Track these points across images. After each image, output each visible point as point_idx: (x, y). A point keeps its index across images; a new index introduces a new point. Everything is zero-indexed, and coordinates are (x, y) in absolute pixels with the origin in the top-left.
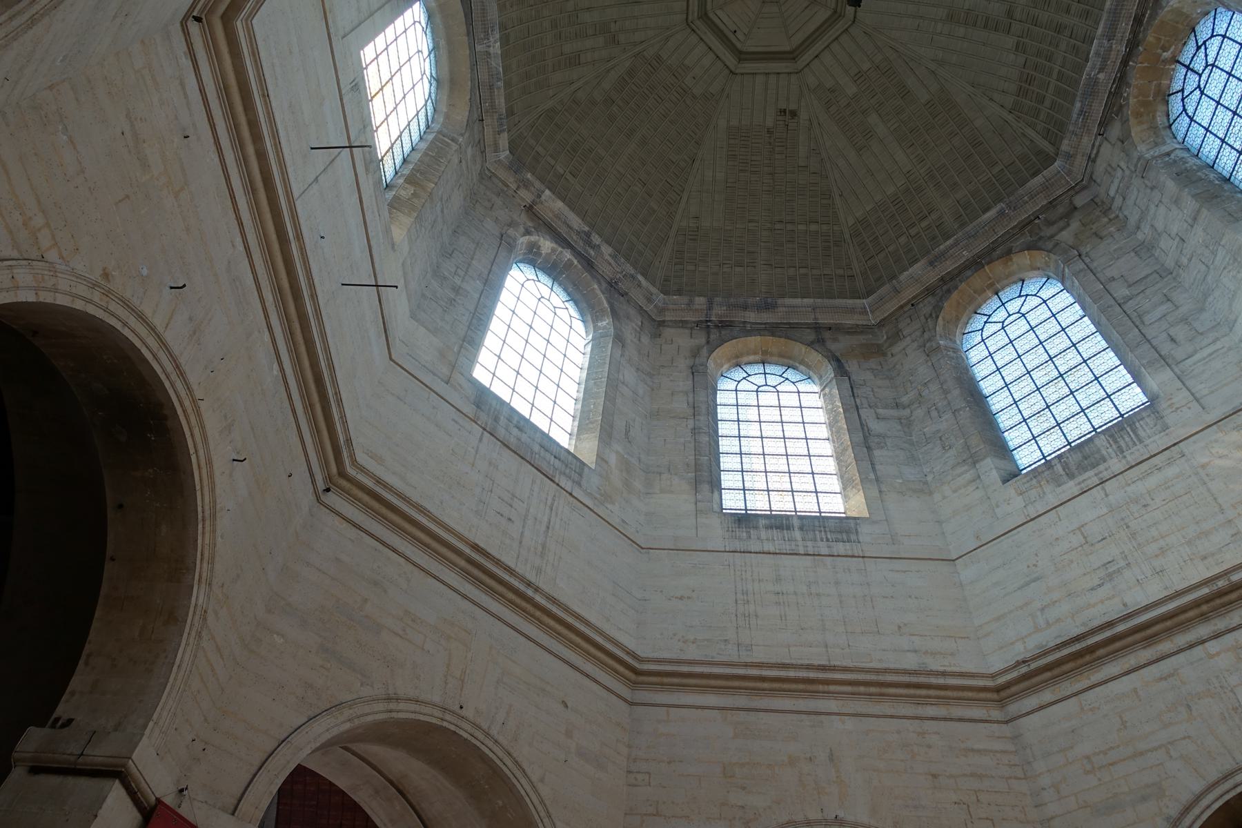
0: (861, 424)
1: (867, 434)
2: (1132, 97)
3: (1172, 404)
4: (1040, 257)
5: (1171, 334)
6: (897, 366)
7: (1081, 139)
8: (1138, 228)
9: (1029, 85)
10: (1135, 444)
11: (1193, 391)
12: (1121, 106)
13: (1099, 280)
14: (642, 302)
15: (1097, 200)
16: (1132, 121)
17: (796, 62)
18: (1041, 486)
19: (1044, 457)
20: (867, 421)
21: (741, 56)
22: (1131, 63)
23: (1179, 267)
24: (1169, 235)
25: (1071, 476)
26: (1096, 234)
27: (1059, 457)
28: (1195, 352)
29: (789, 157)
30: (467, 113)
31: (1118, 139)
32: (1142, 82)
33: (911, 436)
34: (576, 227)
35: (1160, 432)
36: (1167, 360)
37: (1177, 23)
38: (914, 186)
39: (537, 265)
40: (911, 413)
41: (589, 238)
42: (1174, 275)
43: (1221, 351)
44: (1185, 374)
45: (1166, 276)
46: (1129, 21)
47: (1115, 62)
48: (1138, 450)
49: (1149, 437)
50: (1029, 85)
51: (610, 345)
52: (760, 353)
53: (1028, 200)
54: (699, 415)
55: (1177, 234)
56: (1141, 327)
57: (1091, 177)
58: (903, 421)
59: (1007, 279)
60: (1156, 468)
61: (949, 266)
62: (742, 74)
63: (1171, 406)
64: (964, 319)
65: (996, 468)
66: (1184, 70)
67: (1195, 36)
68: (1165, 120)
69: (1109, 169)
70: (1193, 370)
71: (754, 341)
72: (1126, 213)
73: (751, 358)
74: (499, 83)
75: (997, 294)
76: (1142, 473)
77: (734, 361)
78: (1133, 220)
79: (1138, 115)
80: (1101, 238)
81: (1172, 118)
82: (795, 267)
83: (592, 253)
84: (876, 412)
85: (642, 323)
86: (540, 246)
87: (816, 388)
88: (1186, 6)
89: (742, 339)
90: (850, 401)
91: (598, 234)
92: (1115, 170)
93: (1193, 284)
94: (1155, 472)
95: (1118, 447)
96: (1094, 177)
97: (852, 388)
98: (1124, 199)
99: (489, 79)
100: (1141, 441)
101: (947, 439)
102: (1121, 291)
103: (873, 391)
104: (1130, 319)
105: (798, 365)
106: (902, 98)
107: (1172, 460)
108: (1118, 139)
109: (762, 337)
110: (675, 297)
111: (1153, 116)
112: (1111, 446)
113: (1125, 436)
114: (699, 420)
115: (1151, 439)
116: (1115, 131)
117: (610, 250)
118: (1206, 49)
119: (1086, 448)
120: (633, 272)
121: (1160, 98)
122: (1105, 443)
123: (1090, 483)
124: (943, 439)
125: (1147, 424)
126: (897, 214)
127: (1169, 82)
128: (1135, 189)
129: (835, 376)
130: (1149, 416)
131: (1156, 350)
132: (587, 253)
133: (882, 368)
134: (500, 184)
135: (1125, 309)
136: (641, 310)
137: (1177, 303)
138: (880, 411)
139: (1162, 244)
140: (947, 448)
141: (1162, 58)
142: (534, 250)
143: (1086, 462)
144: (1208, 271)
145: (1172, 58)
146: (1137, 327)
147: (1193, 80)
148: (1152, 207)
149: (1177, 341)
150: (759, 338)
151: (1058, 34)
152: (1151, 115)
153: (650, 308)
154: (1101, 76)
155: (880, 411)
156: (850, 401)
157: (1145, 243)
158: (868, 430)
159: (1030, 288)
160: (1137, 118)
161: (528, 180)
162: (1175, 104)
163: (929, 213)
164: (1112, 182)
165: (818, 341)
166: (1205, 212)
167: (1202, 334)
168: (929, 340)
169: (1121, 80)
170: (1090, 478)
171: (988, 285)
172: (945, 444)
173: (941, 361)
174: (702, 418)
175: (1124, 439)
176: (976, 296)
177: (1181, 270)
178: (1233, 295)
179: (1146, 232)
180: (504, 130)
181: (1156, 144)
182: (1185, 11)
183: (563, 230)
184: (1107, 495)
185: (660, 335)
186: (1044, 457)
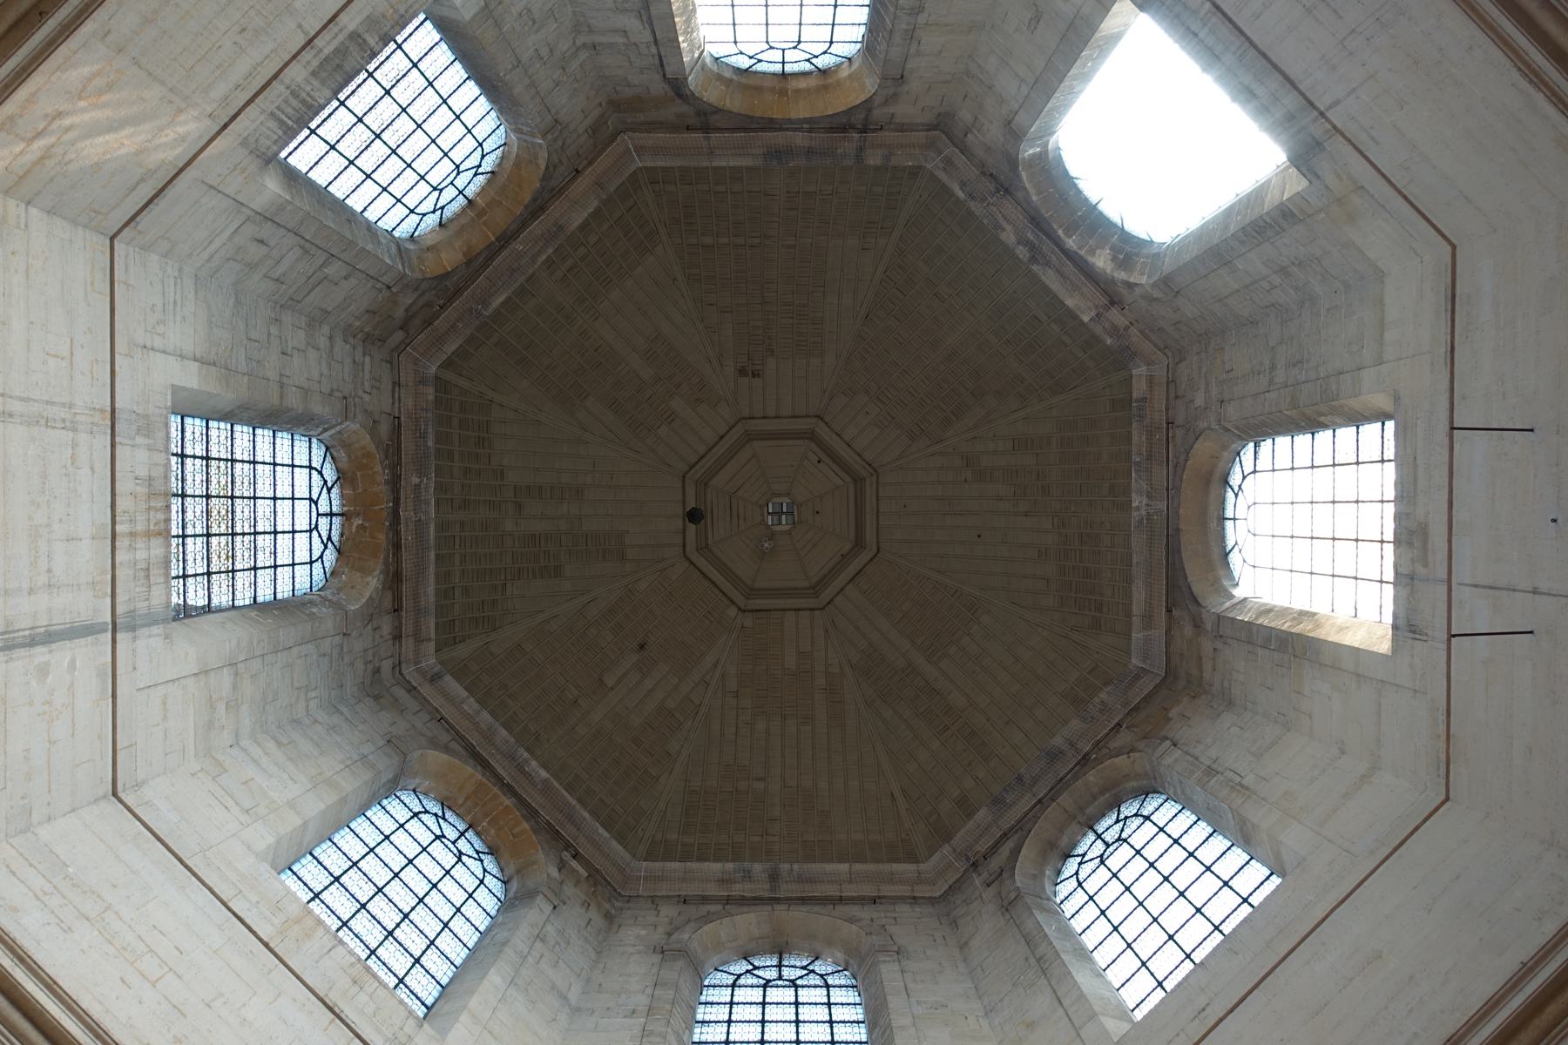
0: (651, 24)
1: (643, 12)
2: (381, 473)
3: (243, 173)
4: (432, 268)
5: (265, 247)
6: (594, 93)
7: (415, 405)
8: (331, 338)
9: (479, 437)
10: (278, 108)
11: (220, 195)
12: (387, 457)
13: (363, 272)
14: (961, 160)
15: (380, 344)
16: (372, 448)
17: (746, 431)
18: (392, 7)
19: (399, 47)
20: (641, 28)
21: (812, 436)
22: (391, 504)
23: (276, 320)
24: (299, 350)
25: (355, 36)
26: (374, 313)
27: (374, 55)
28: (230, 238)
29: (744, 323)
30: (1196, 446)
31: (379, 422)
32: (374, 489)
33: (574, 12)
34: (1050, 272)
35: (249, 135)
36: (262, 218)
37: (360, 559)
38: (588, 303)
39: (1119, 233)
40: (574, 42)
41: (1034, 256)
42: (278, 306)
43: (199, 251)
44: (235, 211)
45: (286, 302)
46: (405, 544)
47: (406, 498)
48: (272, 102)
49: (261, 123)
50: (479, 437)
51: (1032, 130)
52: (790, 93)
53: (458, 324)
54: (906, 31)
55: (292, 356)
56: (302, 242)
57: (391, 363)
58: (587, 29)
59: (463, 226)
60: (242, 87)
61: (536, 228)
62: (808, 416)
63: (244, 170)
64: (508, 165)
65: (457, 9)
66: (335, 509)
67: (335, 547)
68: (335, 454)
69: (378, 384)
70: (228, 218)
71: (800, 111)
72: (348, 347)
73: (803, 84)
74: (1138, 460)
75: (470, 201)
76: (259, 72)
77: (830, 81)
78: (339, 341)
79: (368, 455)
80: (367, 311)
81: (329, 458)
82: (732, 193)
83: (1030, 236)
84: (628, 38)
85: (966, 135)
86: (1112, 260)
87: (709, 48)
88: (360, 580)
89: (817, 115)
90: (666, 51)
91: (1019, 259)
92: (372, 387)
93: (256, 307)
94: (241, 82)
95: (298, 96)
96: (389, 365)
97: (662, 65)
98: (354, 361)
99: (1152, 468)
100: (272, 114)
101: (526, 25)
102: (333, 270)
103: (630, 62)
104: (317, 246)
105: (735, 77)
106: (617, 400)
107: (224, 105)
108: (379, 422)
109: (788, 117)
110: (910, 164)
111: (350, 457)
112: (308, 94)
113: (292, 112)
114: (909, 24)
115: (258, 122)
116: (384, 429)
117: (1003, 236)
118: (322, 541)
119: (340, 79)
120: (972, 204)
121: (349, 475)
122: (316, 94)
123: (326, 35)
124: (531, 23)
125: (268, 138)
126: (604, 267)
127: (344, 492)
128: (347, 379)
129: (686, 79)
130: (268, 148)
131: (278, 224)
132: (1039, 236)
133: (614, 88)
134: (1153, 338)
135: (325, 253)
136: (964, 150)
137: (267, 280)
138: (620, 40)
139: (301, 334)
140: (525, 12)
141: (361, 518)
142: (1121, 257)
143: (337, 61)
144: (247, 334)
145: (351, 518)
146: (307, 241)
147: (324, 508)
148: (325, 372)
149: (256, 243)
150: (793, 116)
151: (465, 500)
152: (353, 458)
153: (950, 150)
154: (415, 480)
155: (620, 40)
156: (666, 51)
157: (318, 324)
158: (641, 16)
159: (432, 220)
160: (369, 452)
161: (1111, 337)
162: (330, 474)
163: (565, 275)
164: (371, 372)
165: (705, 114)
166: (276, 401)
167: (228, 259)
168: (555, 140)
169: (395, 483)
170: (328, 44)
171: (485, 214)
172: (528, 16)
173: (539, 120)
174: (904, 26)
175: (294, 109)
176: (498, 198)
177: (273, 316)
178: (211, 322)
179: (322, 338)
180: (1137, 401)
181: (339, 432)
182: (358, 574)
183: (1070, 268)
184: (300, 26)
185: (939, 115)
186: (399, 47)
